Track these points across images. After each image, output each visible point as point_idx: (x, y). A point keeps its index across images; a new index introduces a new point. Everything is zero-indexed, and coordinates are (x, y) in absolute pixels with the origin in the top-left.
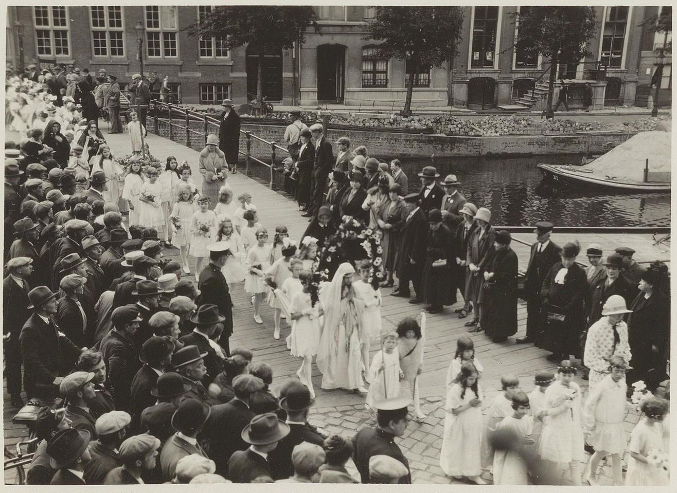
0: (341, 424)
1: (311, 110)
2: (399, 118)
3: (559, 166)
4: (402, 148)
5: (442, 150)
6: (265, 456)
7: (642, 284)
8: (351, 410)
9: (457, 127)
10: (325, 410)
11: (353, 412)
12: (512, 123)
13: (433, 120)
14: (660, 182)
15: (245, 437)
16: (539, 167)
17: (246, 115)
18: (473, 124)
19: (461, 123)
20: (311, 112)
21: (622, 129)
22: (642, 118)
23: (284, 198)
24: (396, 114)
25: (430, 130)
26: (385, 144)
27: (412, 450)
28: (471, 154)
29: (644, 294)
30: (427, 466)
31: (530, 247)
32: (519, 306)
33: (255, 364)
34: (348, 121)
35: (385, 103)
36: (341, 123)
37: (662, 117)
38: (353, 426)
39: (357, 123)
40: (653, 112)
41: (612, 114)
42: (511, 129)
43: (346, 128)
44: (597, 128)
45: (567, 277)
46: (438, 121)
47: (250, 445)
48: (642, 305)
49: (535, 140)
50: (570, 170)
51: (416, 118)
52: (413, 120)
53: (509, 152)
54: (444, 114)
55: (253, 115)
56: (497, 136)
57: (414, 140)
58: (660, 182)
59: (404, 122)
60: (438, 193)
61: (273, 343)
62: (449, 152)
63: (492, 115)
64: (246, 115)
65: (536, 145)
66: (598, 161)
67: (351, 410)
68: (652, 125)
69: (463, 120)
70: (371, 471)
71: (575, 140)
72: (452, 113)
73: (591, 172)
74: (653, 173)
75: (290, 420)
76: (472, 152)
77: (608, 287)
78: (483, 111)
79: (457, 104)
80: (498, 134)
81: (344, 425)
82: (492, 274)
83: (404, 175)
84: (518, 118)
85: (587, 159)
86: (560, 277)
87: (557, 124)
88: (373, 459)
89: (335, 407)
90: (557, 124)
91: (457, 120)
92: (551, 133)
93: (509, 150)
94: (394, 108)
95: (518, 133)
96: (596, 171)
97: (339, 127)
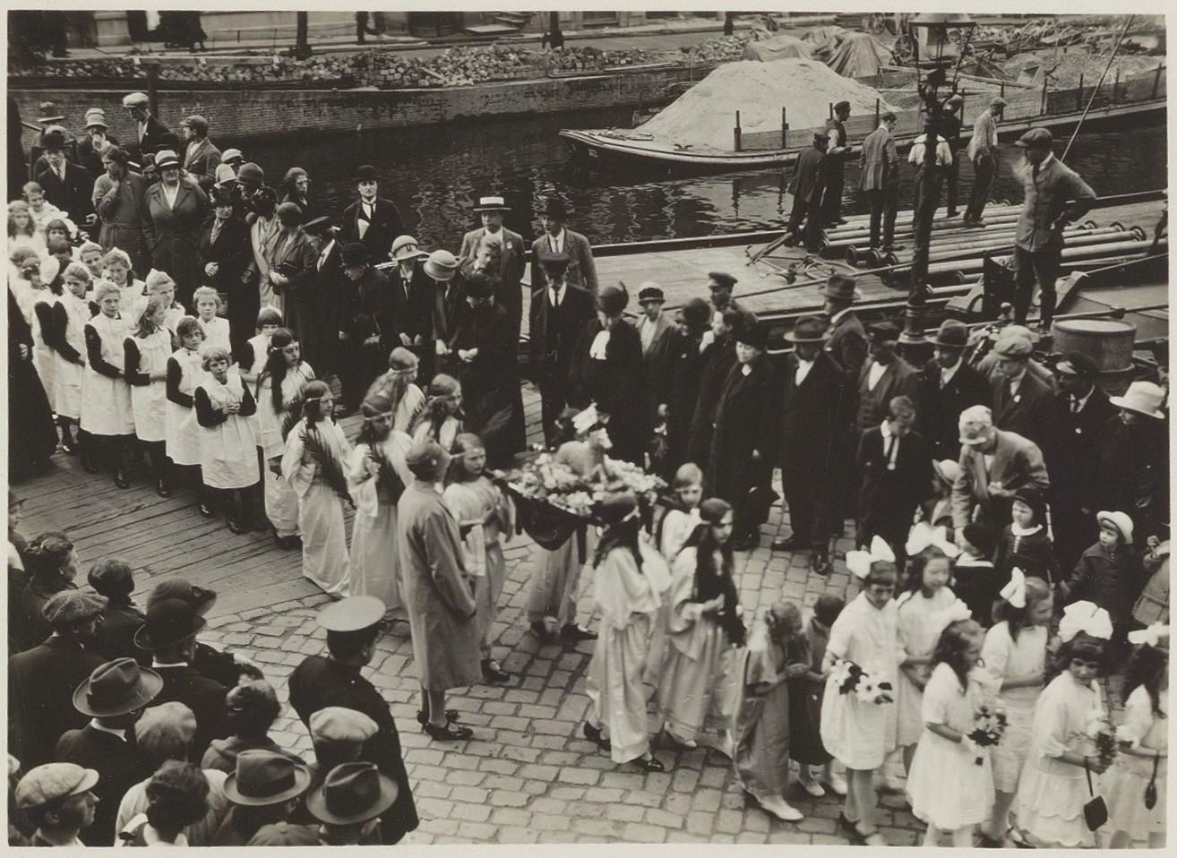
0: (251, 642)
3: (596, 132)
5: (375, 115)
9: (397, 72)
13: (352, 62)
14: (760, 150)
15: (81, 705)
16: (563, 137)
18: (424, 65)
19: (402, 65)
20: (120, 59)
21: (680, 59)
22: (710, 38)
25: (348, 81)
26: (270, 112)
27: (382, 670)
28: (427, 120)
29: (741, 365)
30: (409, 694)
33: (81, 568)
34: (195, 72)
35: (259, 34)
36: (180, 77)
38: (274, 643)
40: (725, 26)
41: (661, 33)
42: (492, 71)
43: (190, 85)
44: (638, 60)
45: (609, 347)
49: (537, 88)
50: (615, 138)
51: (321, 59)
52: (314, 63)
53: (494, 112)
56: (470, 85)
57: (323, 101)
59: (300, 70)
62: (388, 119)
63: (455, 46)
66: (659, 119)
68: (726, 49)
69: (405, 58)
72: (384, 46)
73: (650, 138)
74: (748, 135)
75: (158, 662)
76: (431, 117)
78: (439, 39)
79: (392, 28)
80: (470, 81)
81: (258, 642)
82: (474, 351)
84: (502, 48)
85: (641, 115)
86: (599, 347)
88: (315, 719)
89: (237, 614)
90: (571, 57)
91: (396, 59)
92: (563, 74)
93: (492, 109)
94: (278, 42)
95: (506, 76)
96: (659, 135)
97: (180, 85)
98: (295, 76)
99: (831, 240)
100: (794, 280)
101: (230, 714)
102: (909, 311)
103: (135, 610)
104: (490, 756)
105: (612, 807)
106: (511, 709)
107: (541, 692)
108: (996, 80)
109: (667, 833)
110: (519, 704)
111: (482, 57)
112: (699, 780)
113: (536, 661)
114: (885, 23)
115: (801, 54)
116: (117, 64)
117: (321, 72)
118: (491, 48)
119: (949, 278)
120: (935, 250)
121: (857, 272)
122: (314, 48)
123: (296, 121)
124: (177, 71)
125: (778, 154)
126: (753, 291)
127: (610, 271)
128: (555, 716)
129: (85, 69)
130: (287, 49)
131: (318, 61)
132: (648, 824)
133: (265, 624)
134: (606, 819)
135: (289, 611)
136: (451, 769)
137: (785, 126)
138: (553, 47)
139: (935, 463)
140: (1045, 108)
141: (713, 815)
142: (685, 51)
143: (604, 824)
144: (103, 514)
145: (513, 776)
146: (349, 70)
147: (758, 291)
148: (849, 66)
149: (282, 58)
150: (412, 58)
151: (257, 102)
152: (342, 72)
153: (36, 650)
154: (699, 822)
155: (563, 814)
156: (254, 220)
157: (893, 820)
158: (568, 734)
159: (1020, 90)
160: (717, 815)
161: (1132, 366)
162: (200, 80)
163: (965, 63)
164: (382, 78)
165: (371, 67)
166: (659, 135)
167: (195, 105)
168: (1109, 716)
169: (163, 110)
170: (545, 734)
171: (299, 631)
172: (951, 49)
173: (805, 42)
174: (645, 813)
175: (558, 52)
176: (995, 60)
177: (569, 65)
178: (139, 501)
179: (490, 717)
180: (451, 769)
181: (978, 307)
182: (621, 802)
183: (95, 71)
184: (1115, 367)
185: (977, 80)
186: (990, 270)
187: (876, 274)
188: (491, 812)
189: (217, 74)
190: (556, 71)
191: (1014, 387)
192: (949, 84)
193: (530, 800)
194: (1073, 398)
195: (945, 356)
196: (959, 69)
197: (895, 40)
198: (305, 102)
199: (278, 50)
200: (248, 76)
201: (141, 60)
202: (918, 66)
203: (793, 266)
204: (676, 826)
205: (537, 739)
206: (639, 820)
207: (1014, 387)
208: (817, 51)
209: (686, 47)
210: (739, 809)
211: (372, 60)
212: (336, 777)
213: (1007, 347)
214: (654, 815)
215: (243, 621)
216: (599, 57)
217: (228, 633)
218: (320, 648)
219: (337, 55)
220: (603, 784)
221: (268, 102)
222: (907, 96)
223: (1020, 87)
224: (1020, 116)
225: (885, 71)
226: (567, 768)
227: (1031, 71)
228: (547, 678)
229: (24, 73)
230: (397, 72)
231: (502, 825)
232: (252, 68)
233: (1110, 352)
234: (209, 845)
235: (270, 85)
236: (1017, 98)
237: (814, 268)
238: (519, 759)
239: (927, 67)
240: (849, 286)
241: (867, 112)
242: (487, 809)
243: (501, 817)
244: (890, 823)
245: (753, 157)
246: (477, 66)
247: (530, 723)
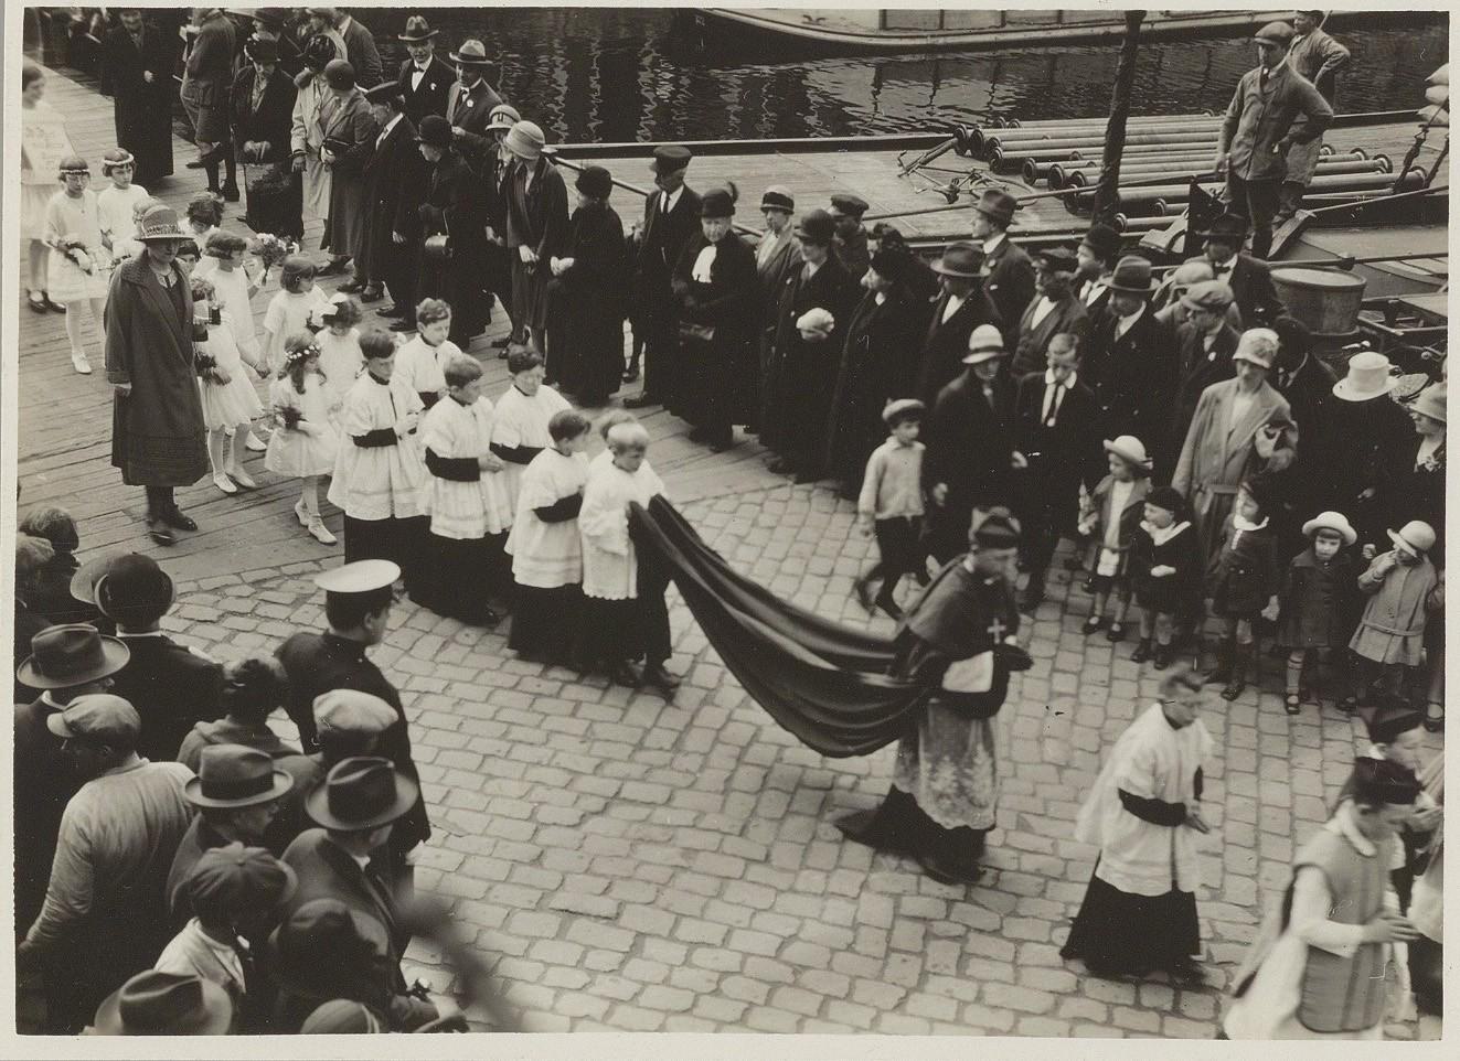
0: (253, 610)
14: (910, 29)
23: (78, 86)
27: (412, 652)
29: (874, 293)
30: (445, 683)
38: (283, 612)
45: (716, 267)
48: (870, 317)
58: (910, 29)
60: (441, 75)
70: (320, 728)
77: (807, 281)
81: (261, 611)
82: (569, 261)
83: (362, 27)
86: (703, 268)
88: (320, 704)
89: (238, 574)
100: (957, 198)
104: (539, 763)
105: (681, 832)
112: (789, 805)
119: (1147, 207)
120: (1128, 168)
121: (1035, 192)
125: (932, 36)
126: (904, 211)
128: (621, 720)
132: (724, 853)
133: (272, 589)
134: (674, 846)
135: (303, 573)
143: (669, 851)
145: (565, 788)
147: (910, 210)
154: (785, 855)
156: (305, 83)
158: (635, 741)
160: (807, 848)
161: (1357, 329)
168: (1289, 753)
171: (313, 600)
174: (722, 840)
179: (541, 717)
180: (490, 777)
181: (1179, 247)
182: (694, 826)
184: (1335, 330)
186: (1197, 200)
188: (536, 830)
191: (1208, 342)
194: (1281, 370)
195: (1120, 301)
203: (956, 180)
204: (758, 858)
207: (1208, 342)
210: (836, 841)
212: (341, 774)
213: (1202, 295)
214: (732, 844)
217: (225, 596)
218: (318, 623)
220: (674, 804)
233: (1332, 311)
237: (982, 185)
238: (575, 768)
242: (531, 827)
245: (901, 37)
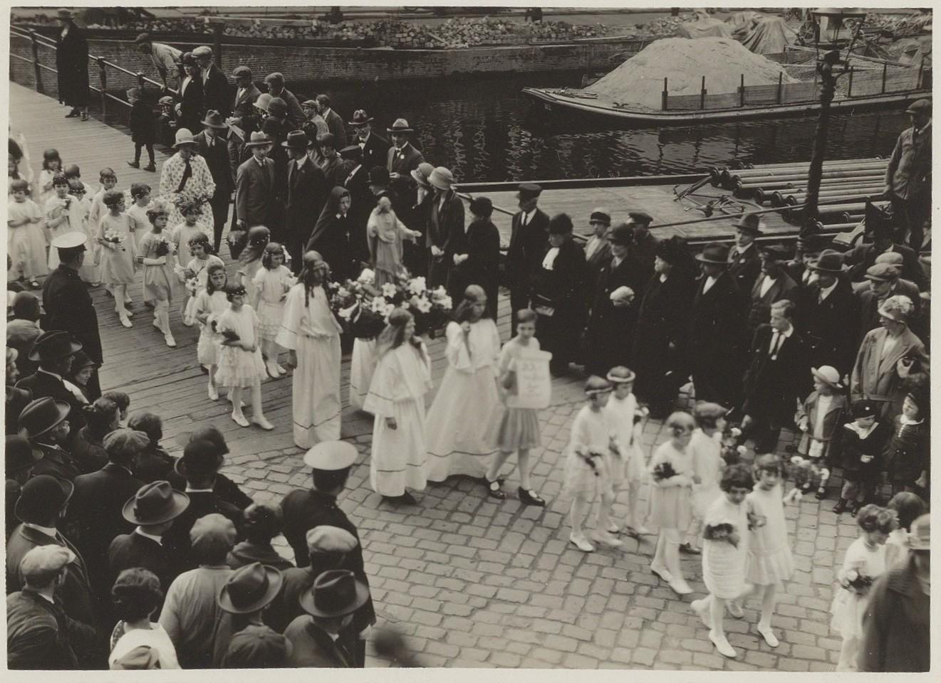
1: (194, 15)
2: (325, 25)
3: (552, 91)
4: (332, 70)
6: (158, 539)
7: (659, 263)
8: (279, 456)
9: (409, 36)
10: (244, 459)
11: (282, 459)
12: (485, 29)
13: (373, 27)
15: (129, 515)
17: (96, 26)
18: (430, 31)
19: (413, 31)
20: (194, 18)
21: (634, 34)
24: (319, 19)
25: (370, 41)
27: (364, 504)
29: (659, 274)
30: (385, 524)
31: (512, 217)
32: (501, 297)
33: (135, 411)
34: (252, 30)
36: (240, 34)
37: (685, 16)
38: (283, 478)
39: (265, 34)
42: (483, 37)
44: (601, 33)
45: (556, 261)
46: (381, 29)
47: (136, 526)
51: (349, 24)
52: (344, 27)
54: (388, 17)
55: (106, 25)
56: (466, 48)
61: (160, 371)
64: (96, 26)
65: (520, 60)
67: (279, 456)
68: (672, 27)
71: (572, 51)
73: (594, 97)
75: (192, 488)
82: (464, 256)
83: (336, 115)
85: (589, 78)
87: (547, 29)
88: (310, 535)
89: (256, 454)
90: (547, 29)
91: (408, 26)
92: (540, 42)
95: (494, 42)
96: (602, 95)
97: (240, 40)
98: (329, 36)
99: (744, 183)
100: (711, 214)
101: (247, 525)
102: (799, 243)
103: (162, 452)
104: (444, 576)
105: (536, 621)
106: (463, 540)
107: (487, 528)
108: (881, 59)
109: (578, 644)
110: (470, 537)
111: (477, 26)
113: (485, 504)
114: (796, 12)
115: (723, 35)
116: (191, 22)
117: (349, 34)
118: (484, 20)
120: (823, 193)
121: (762, 209)
122: (344, 15)
123: (327, 72)
124: (238, 29)
127: (565, 200)
128: (497, 548)
129: (166, 26)
130: (324, 15)
131: (347, 25)
133: (278, 463)
136: (413, 584)
137: (704, 91)
138: (533, 20)
139: (813, 370)
140: (921, 83)
141: (615, 632)
142: (639, 27)
144: (160, 371)
145: (461, 592)
146: (371, 33)
148: (761, 45)
149: (319, 22)
150: (421, 25)
151: (298, 55)
152: (366, 34)
153: (97, 474)
155: (498, 624)
157: (759, 645)
159: (900, 68)
162: (255, 37)
163: (856, 45)
164: (397, 40)
165: (388, 31)
166: (602, 95)
167: (250, 57)
169: (225, 60)
170: (488, 561)
172: (846, 34)
173: (727, 24)
175: (537, 24)
176: (882, 44)
177: (545, 35)
178: (187, 363)
180: (413, 584)
182: (544, 618)
183: (174, 28)
185: (864, 60)
187: (778, 211)
188: (442, 619)
189: (268, 32)
190: (534, 40)
192: (842, 63)
193: (473, 611)
196: (851, 50)
197: (801, 25)
198: (335, 57)
199: (317, 16)
200: (292, 35)
201: (210, 19)
202: (817, 47)
203: (711, 203)
205: (481, 564)
206: (558, 632)
208: (736, 31)
209: (640, 24)
211: (389, 26)
212: (322, 581)
215: (260, 460)
216: (570, 30)
219: (361, 21)
220: (532, 603)
221: (306, 56)
222: (806, 70)
223: (901, 66)
224: (899, 90)
225: (791, 49)
226: (504, 589)
227: (911, 53)
228: (493, 518)
229: (120, 27)
230: (409, 36)
231: (450, 629)
232: (296, 28)
234: (931, 78)
235: (309, 43)
236: (898, 75)
237: (728, 205)
239: (826, 48)
240: (753, 219)
241: (771, 83)
243: (449, 623)
244: (757, 648)
246: (472, 33)
247: (477, 552)
